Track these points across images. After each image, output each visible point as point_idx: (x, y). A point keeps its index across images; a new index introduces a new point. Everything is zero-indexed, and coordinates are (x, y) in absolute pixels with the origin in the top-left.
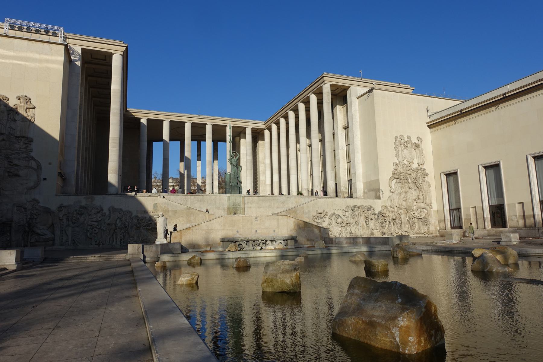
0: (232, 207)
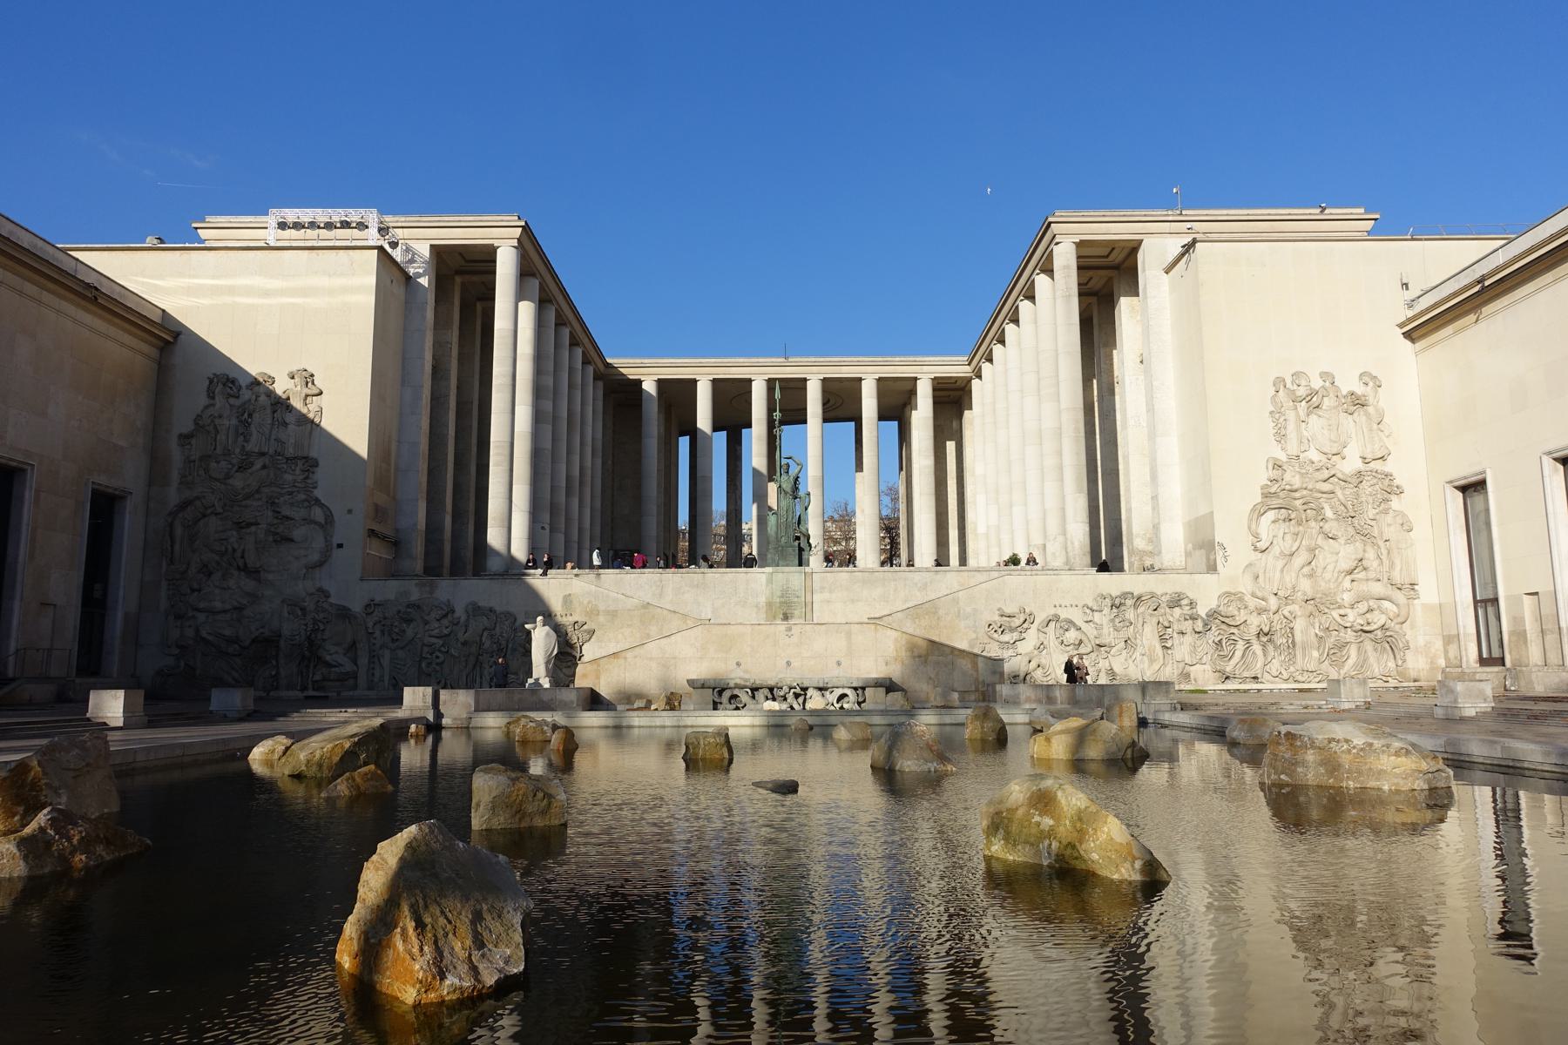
0: (778, 600)
